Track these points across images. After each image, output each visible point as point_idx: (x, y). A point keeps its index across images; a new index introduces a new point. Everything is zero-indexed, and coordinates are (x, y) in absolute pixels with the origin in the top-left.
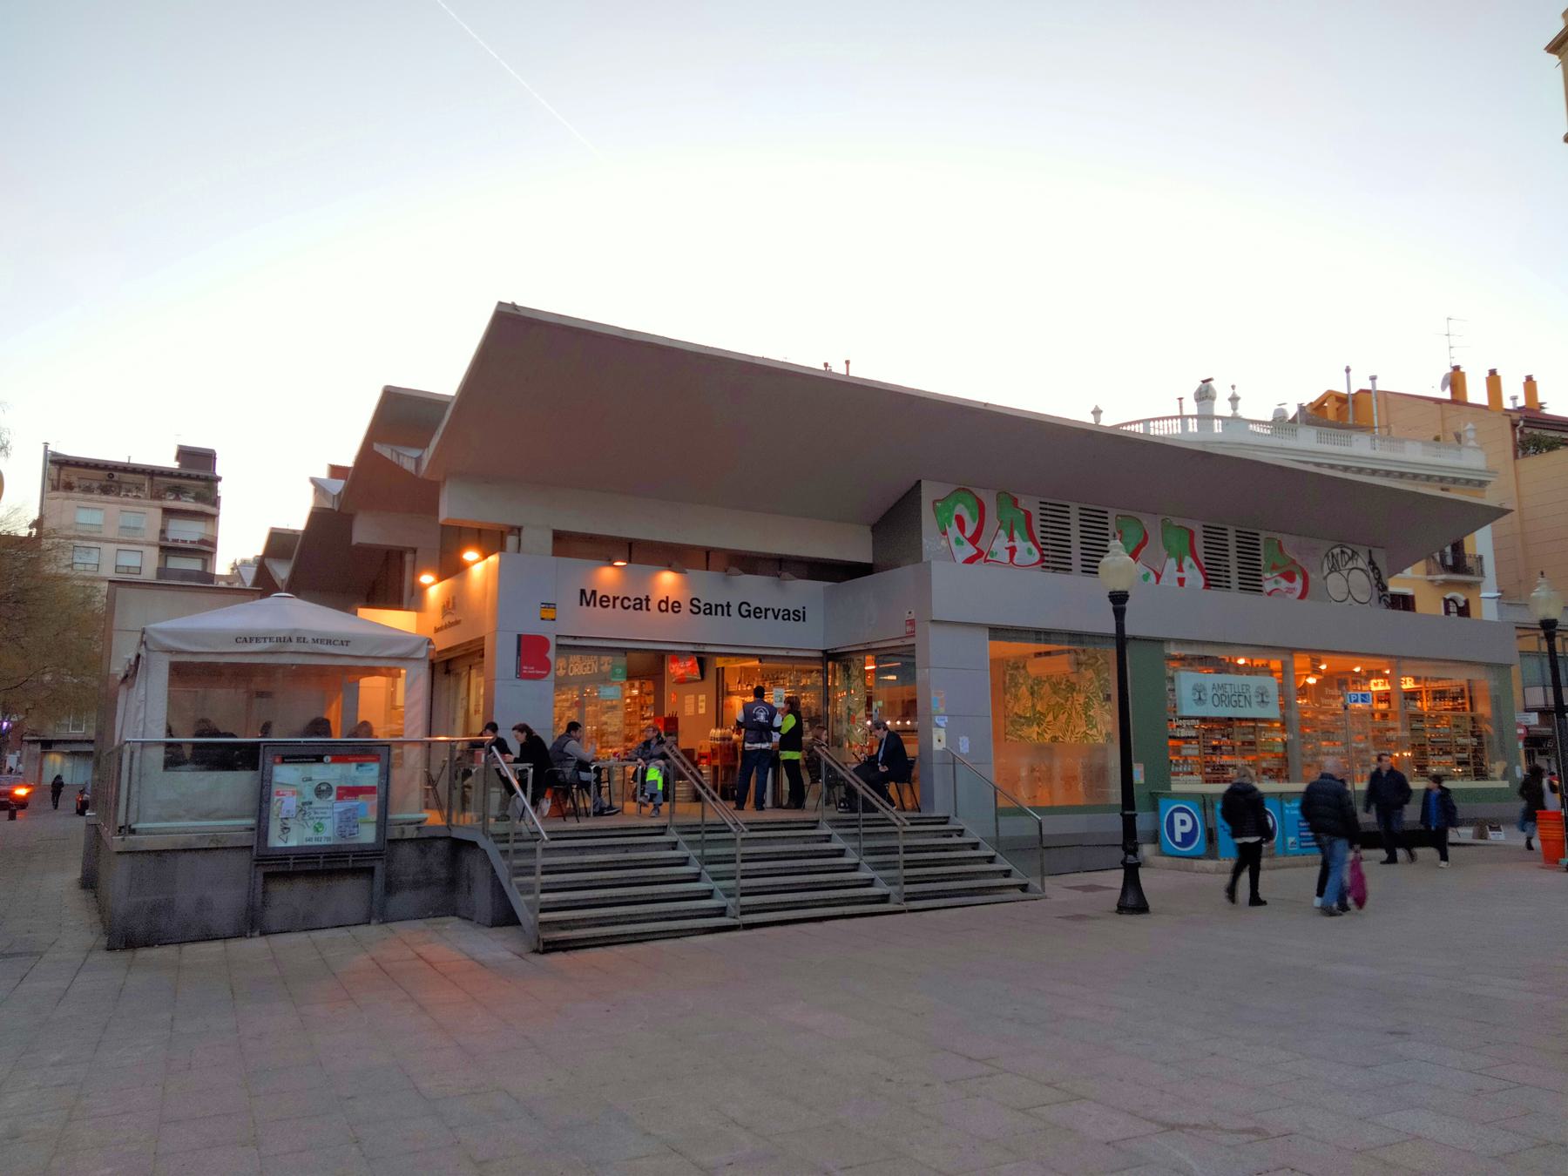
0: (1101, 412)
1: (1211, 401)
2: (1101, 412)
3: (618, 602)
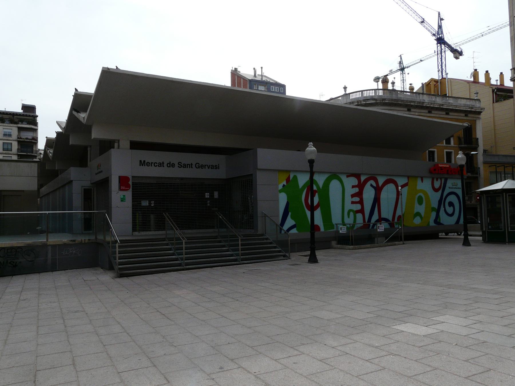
0: (347, 88)
1: (387, 83)
2: (347, 88)
3: (153, 164)
